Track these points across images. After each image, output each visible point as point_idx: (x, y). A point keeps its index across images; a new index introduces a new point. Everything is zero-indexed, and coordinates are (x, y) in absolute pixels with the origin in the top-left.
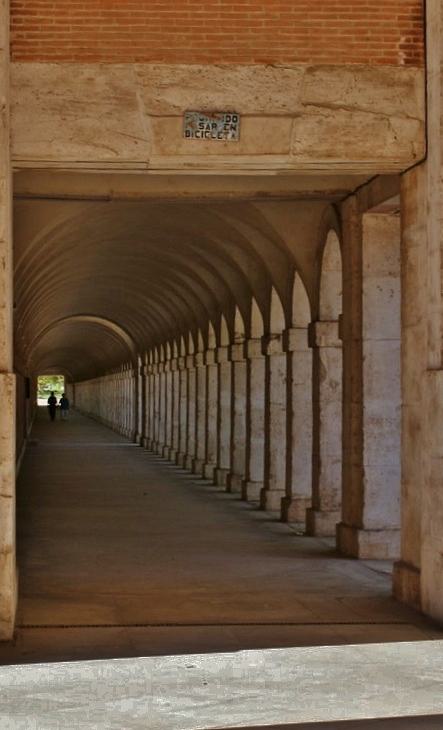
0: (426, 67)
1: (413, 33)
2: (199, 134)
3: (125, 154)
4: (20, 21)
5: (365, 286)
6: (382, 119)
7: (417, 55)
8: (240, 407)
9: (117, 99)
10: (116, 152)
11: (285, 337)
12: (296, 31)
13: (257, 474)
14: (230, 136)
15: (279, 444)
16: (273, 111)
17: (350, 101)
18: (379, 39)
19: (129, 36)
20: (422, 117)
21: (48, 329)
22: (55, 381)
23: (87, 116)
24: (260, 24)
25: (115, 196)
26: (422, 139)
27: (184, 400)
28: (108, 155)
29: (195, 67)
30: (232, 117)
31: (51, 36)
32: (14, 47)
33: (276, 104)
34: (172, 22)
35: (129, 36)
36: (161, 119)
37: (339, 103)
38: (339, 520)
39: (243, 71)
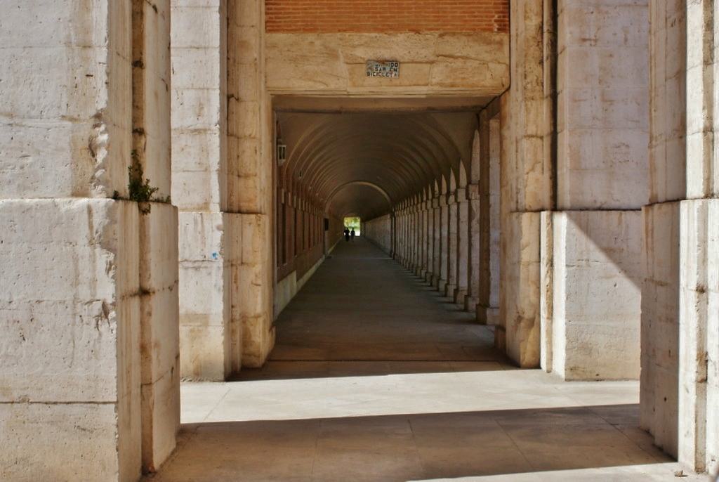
0: (510, 33)
1: (502, 12)
2: (375, 74)
3: (332, 86)
4: (271, 9)
5: (491, 163)
6: (484, 64)
7: (505, 25)
8: (437, 236)
9: (328, 54)
10: (325, 84)
11: (456, 193)
12: (433, 13)
13: (444, 276)
14: (393, 75)
15: (454, 257)
16: (419, 60)
17: (464, 53)
18: (482, 17)
19: (335, 17)
20: (508, 63)
21: (337, 191)
22: (356, 221)
23: (311, 65)
24: (411, 8)
25: (344, 110)
26: (508, 75)
27: (413, 231)
28: (322, 87)
29: (373, 35)
30: (395, 64)
31: (289, 17)
32: (268, 24)
33: (421, 56)
34: (359, 8)
35: (335, 17)
36: (354, 65)
37: (459, 54)
38: (478, 303)
39: (401, 37)
